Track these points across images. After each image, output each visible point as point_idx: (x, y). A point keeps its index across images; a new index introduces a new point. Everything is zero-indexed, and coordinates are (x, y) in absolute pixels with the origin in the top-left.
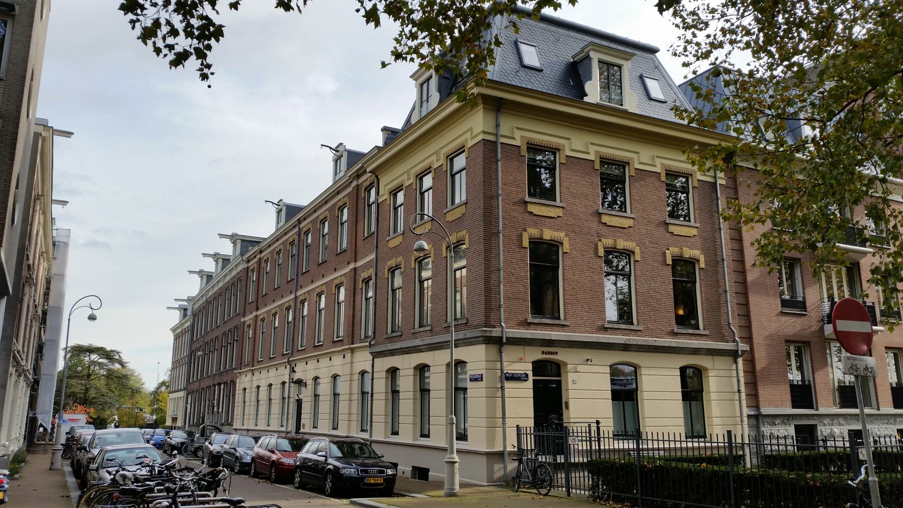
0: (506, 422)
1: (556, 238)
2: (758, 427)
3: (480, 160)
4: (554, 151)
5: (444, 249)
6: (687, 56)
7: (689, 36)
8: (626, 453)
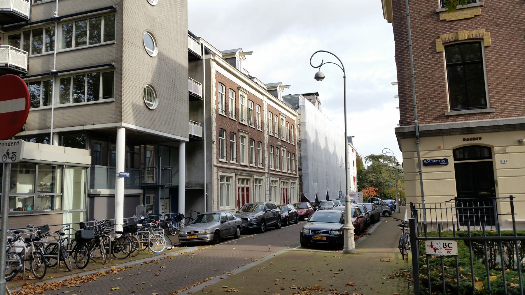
0: (424, 199)
1: (447, 39)
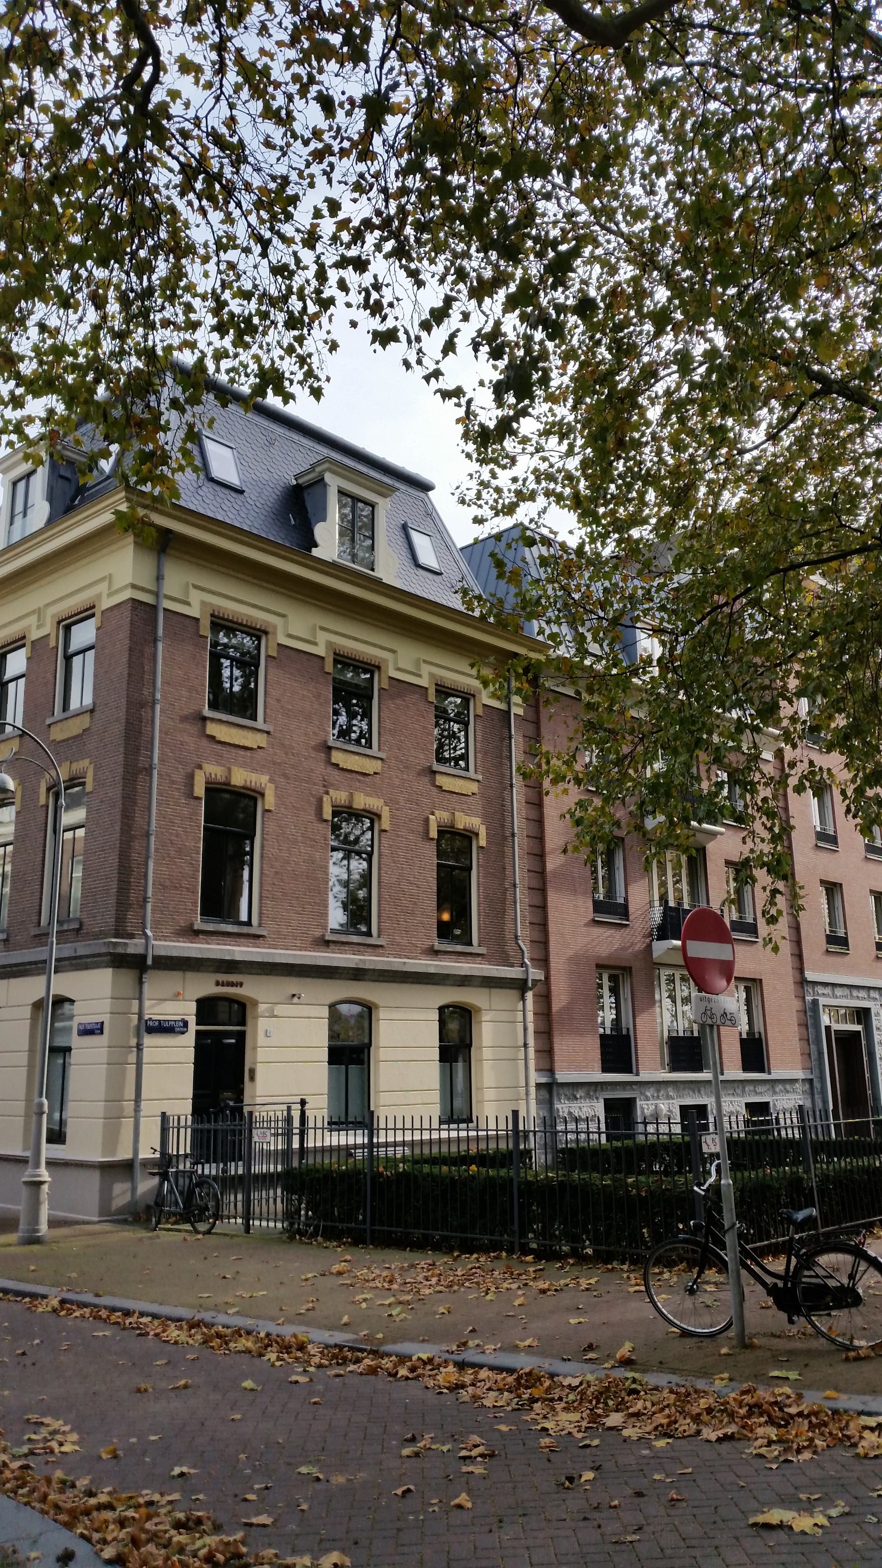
2: (551, 1103)
3: (123, 636)
4: (258, 633)
5: (43, 789)
6: (480, 506)
7: (486, 476)
8: (343, 1153)
